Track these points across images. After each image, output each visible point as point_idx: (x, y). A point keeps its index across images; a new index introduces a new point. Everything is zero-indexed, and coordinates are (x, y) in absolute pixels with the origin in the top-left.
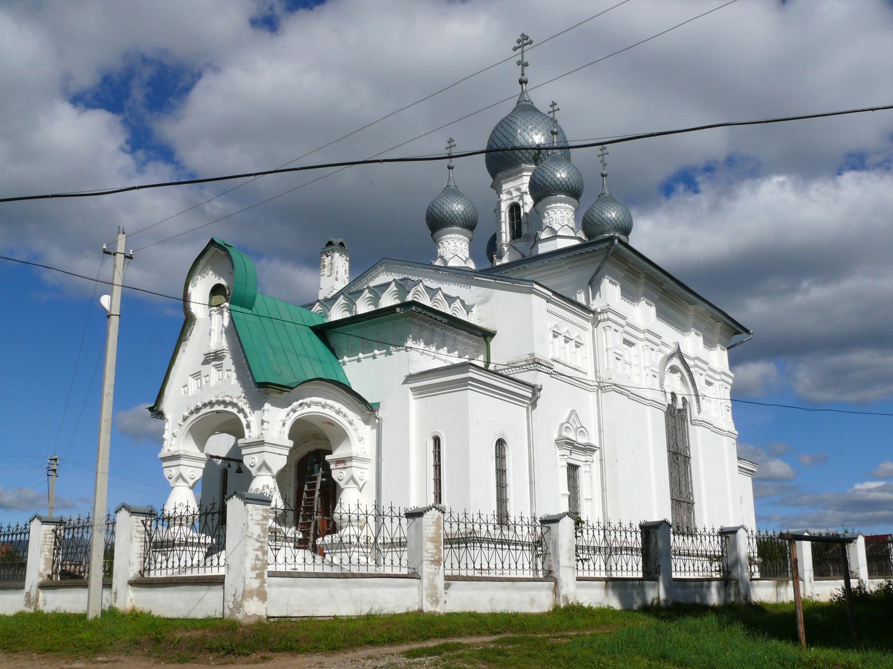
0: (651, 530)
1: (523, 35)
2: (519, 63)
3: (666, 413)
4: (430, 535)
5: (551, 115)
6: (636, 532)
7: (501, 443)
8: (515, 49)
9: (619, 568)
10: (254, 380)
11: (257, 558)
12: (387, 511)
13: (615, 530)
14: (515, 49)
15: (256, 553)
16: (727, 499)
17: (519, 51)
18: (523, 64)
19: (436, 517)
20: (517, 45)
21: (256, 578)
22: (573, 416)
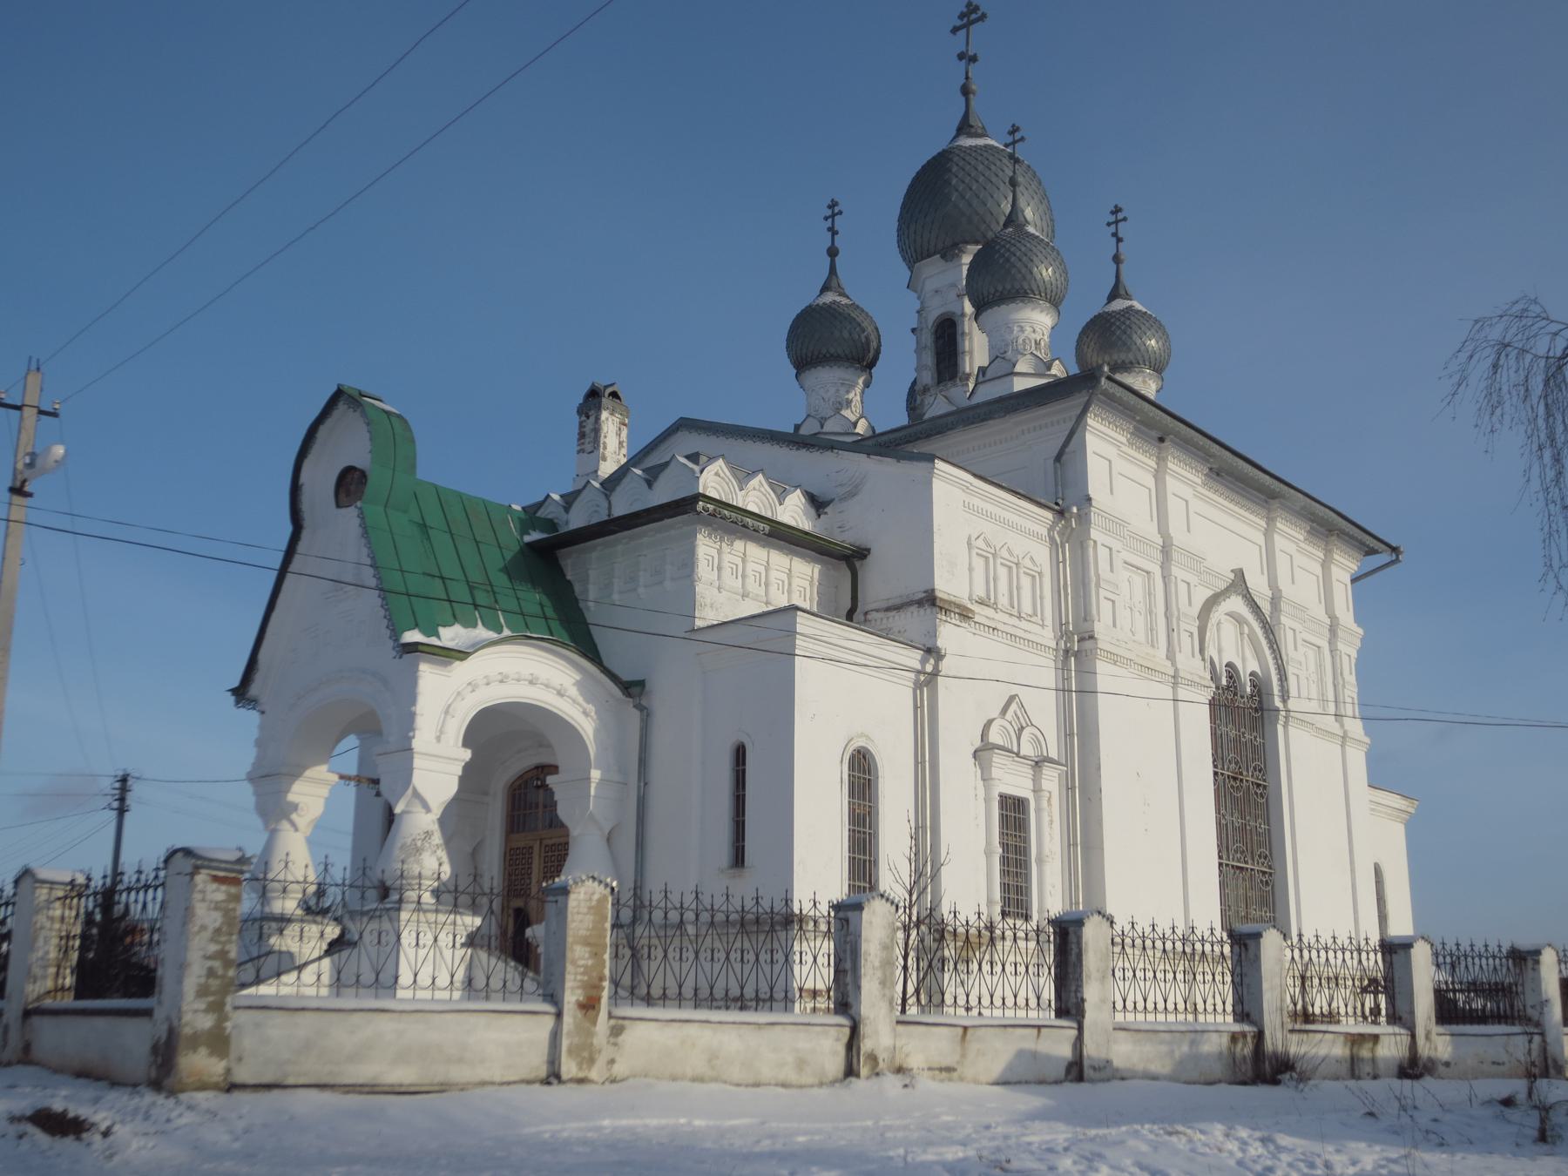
0: (1071, 929)
1: (969, 4)
2: (961, 56)
3: (1213, 704)
4: (583, 932)
5: (1009, 150)
6: (1375, 951)
7: (740, 754)
8: (955, 30)
9: (998, 1002)
10: (927, 682)
11: (211, 973)
12: (657, 898)
13: (1326, 949)
14: (955, 30)
15: (210, 963)
16: (1351, 870)
17: (963, 32)
18: (968, 58)
19: (596, 897)
20: (959, 23)
21: (207, 1011)
22: (1014, 707)
